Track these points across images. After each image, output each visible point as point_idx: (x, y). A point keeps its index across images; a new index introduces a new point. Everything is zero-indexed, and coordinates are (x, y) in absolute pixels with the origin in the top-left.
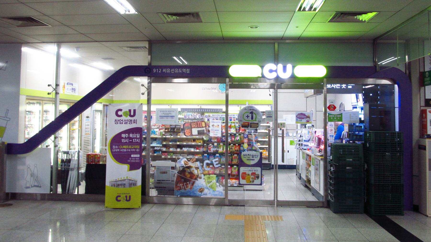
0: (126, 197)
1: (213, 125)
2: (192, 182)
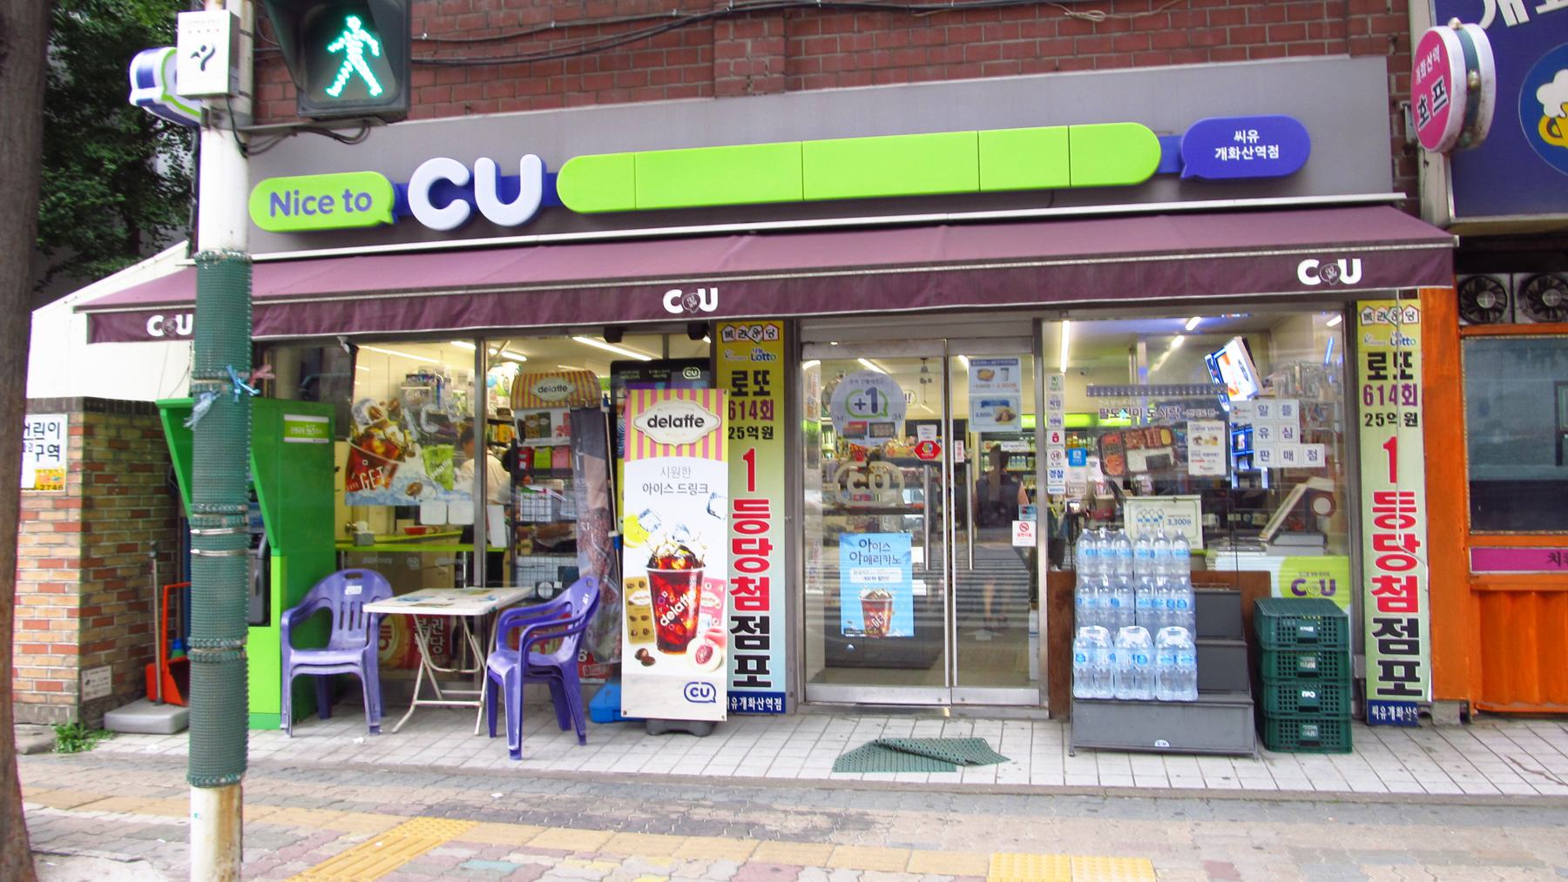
0: (1322, 582)
1: (1197, 440)
2: (388, 467)
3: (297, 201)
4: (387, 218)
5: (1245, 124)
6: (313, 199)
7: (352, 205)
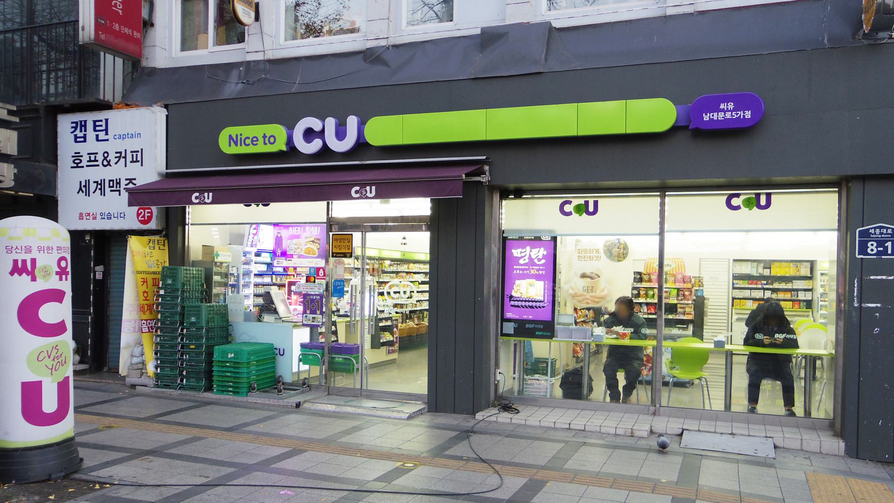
4: (284, 148)
5: (726, 100)
6: (248, 138)
7: (267, 141)
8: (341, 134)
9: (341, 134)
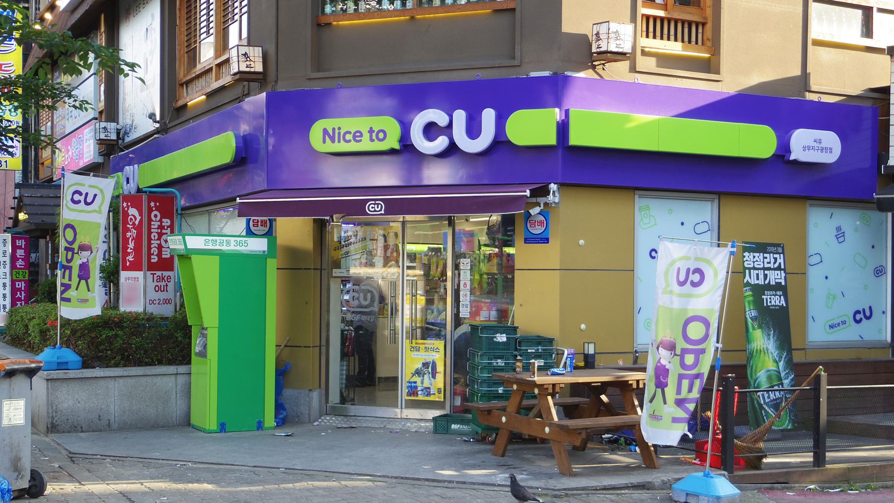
3: (339, 133)
6: (349, 133)
8: (473, 131)
9: (473, 131)
